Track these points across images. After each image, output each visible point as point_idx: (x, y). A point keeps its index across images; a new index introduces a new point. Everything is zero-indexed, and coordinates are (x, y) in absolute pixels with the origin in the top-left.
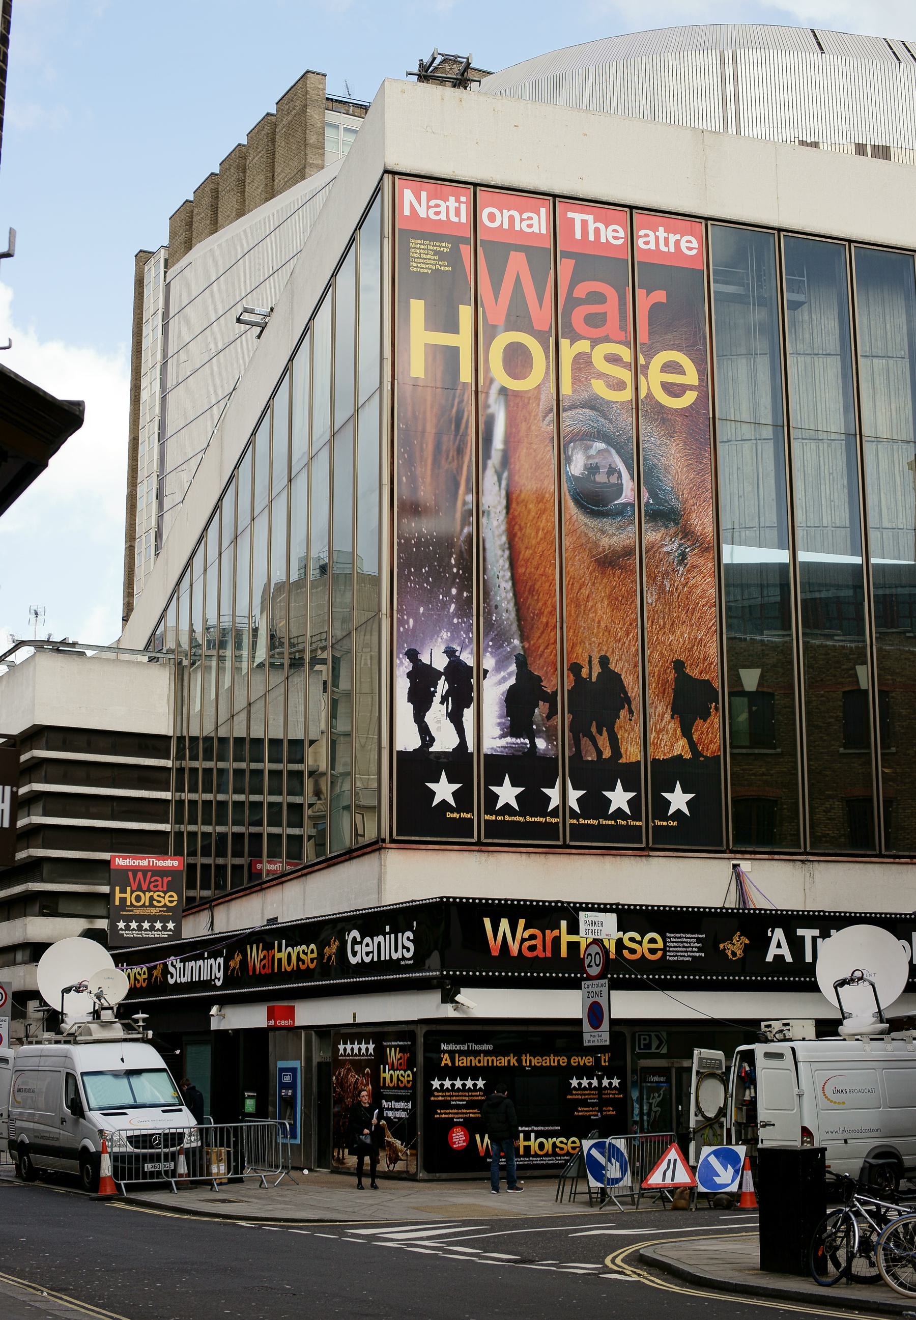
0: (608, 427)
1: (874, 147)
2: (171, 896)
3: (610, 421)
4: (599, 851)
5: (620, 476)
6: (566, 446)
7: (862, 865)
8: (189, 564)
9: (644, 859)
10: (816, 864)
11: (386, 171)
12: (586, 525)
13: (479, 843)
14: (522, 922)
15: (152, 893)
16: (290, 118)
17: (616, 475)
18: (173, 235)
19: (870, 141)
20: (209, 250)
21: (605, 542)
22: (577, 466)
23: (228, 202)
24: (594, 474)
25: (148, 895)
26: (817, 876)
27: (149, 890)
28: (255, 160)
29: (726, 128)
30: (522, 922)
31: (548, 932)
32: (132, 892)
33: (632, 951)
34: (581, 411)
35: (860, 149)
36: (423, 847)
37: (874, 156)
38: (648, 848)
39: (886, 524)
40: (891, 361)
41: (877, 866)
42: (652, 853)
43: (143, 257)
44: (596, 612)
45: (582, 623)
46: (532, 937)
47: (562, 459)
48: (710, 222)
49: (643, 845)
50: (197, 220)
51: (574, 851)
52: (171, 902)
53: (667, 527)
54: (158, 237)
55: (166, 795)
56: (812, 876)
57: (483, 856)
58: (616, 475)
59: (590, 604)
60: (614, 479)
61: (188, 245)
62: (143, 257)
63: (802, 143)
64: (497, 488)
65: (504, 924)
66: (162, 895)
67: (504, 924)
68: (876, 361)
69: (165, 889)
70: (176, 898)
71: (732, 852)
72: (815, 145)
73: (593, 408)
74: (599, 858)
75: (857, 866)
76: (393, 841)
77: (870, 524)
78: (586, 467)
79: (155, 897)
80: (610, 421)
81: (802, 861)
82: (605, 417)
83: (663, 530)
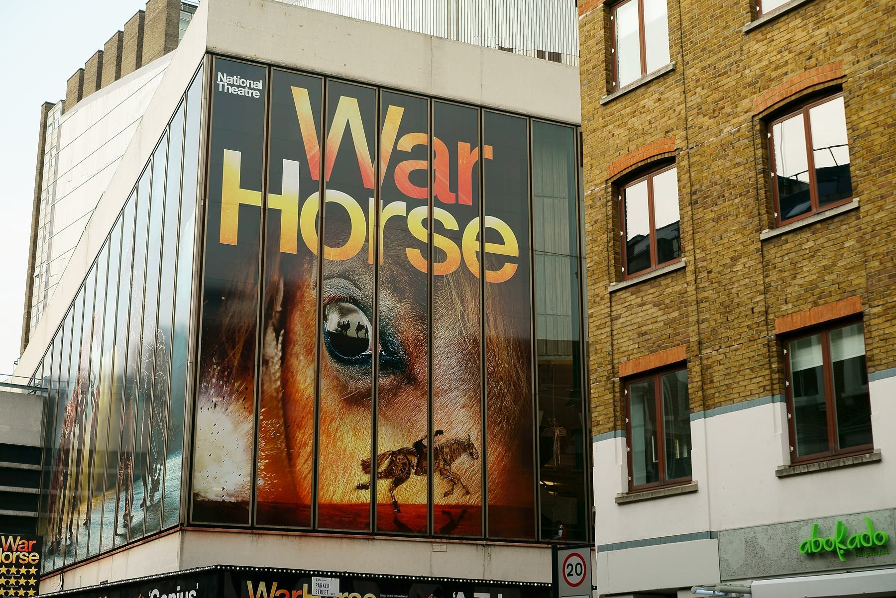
0: (358, 295)
1: (550, 53)
2: (34, 556)
3: (360, 289)
4: (338, 535)
5: (367, 332)
6: (325, 307)
7: (525, 549)
8: (62, 324)
9: (370, 542)
10: (492, 548)
11: (207, 52)
12: (338, 371)
13: (252, 528)
14: (275, 585)
15: (398, 208)
16: (155, 14)
17: (364, 330)
18: (69, 92)
19: (547, 49)
20: (95, 104)
21: (352, 385)
22: (333, 322)
23: (109, 70)
24: (346, 331)
25: (15, 554)
26: (493, 555)
27: (17, 551)
28: (130, 44)
29: (449, 35)
30: (275, 585)
31: (463, 147)
32: (306, 188)
33: (24, 560)
34: (337, 280)
35: (541, 54)
36: (211, 529)
37: (550, 59)
38: (373, 534)
39: (549, 312)
40: (556, 201)
41: (536, 550)
42: (376, 537)
43: (48, 106)
44: (342, 440)
45: (331, 450)
46: (23, 543)
47: (323, 318)
48: (433, 100)
49: (370, 532)
50: (87, 82)
51: (320, 534)
52: (33, 560)
53: (395, 374)
54: (58, 93)
55: (33, 491)
56: (490, 556)
57: (255, 538)
58: (364, 330)
59: (339, 434)
60: (361, 334)
61: (80, 98)
62: (48, 106)
63: (501, 48)
64: (275, 343)
65: (262, 586)
66: (450, 222)
67: (262, 586)
68: (545, 199)
69: (466, 198)
70: (38, 557)
71: (433, 537)
72: (510, 50)
73: (346, 278)
74: (339, 541)
75: (522, 549)
76: (189, 525)
77: (537, 311)
78: (339, 324)
79: (21, 556)
80: (360, 289)
81: (483, 545)
82: (356, 285)
83: (392, 377)
